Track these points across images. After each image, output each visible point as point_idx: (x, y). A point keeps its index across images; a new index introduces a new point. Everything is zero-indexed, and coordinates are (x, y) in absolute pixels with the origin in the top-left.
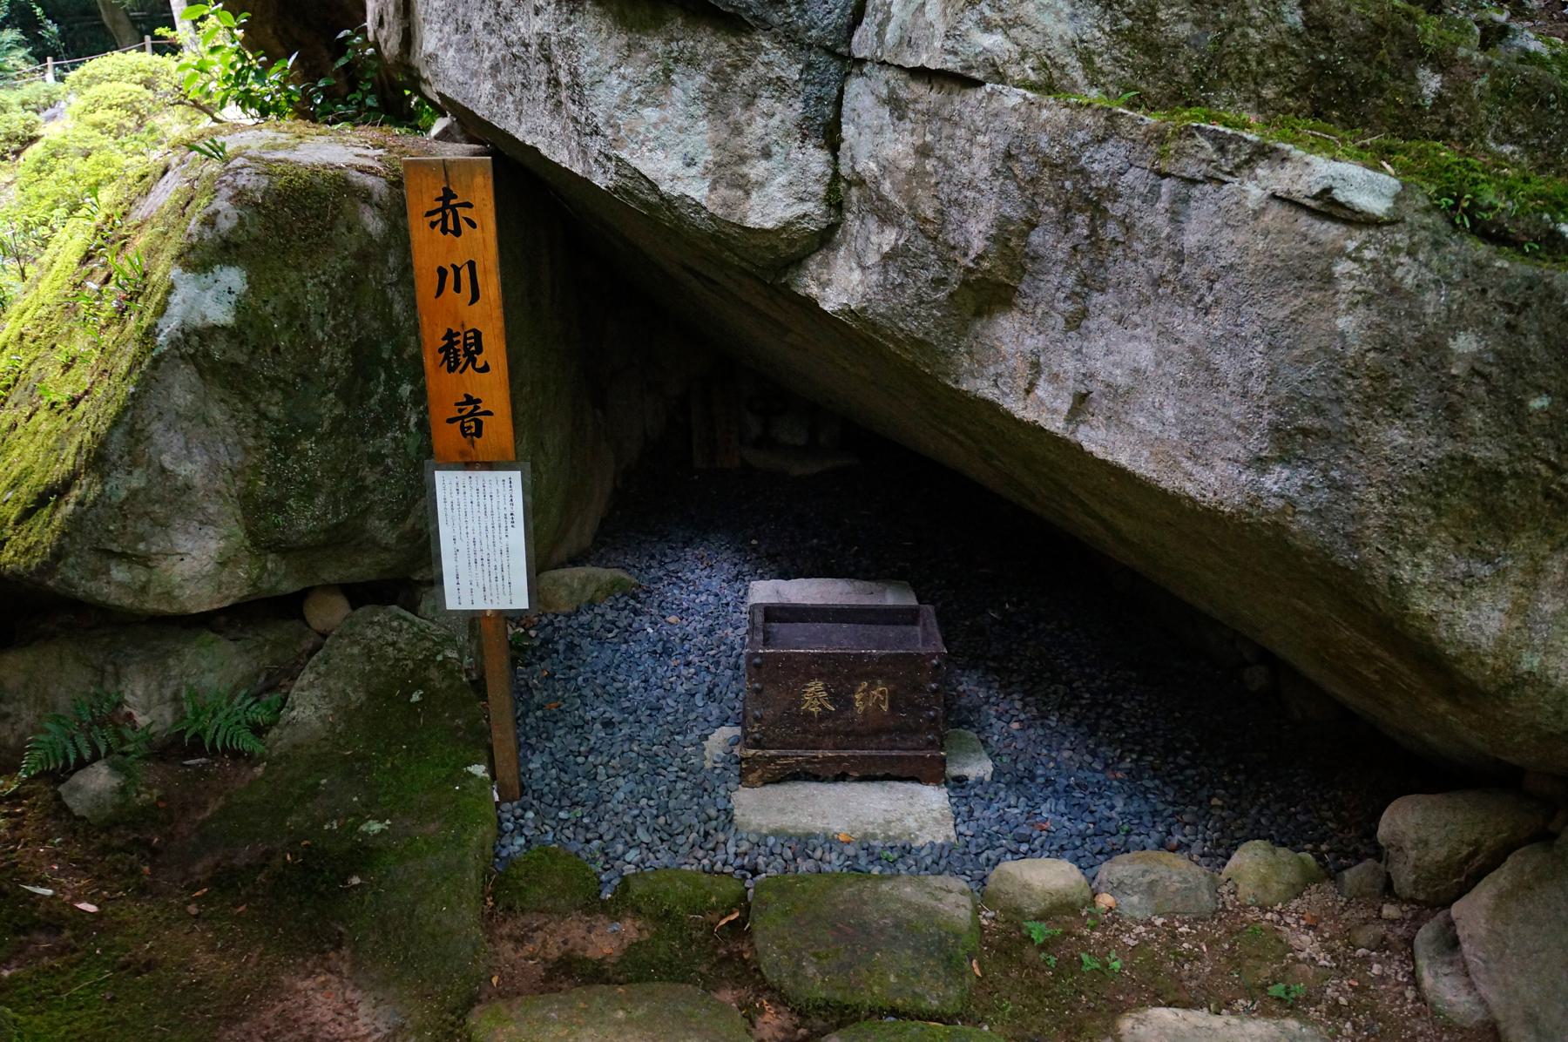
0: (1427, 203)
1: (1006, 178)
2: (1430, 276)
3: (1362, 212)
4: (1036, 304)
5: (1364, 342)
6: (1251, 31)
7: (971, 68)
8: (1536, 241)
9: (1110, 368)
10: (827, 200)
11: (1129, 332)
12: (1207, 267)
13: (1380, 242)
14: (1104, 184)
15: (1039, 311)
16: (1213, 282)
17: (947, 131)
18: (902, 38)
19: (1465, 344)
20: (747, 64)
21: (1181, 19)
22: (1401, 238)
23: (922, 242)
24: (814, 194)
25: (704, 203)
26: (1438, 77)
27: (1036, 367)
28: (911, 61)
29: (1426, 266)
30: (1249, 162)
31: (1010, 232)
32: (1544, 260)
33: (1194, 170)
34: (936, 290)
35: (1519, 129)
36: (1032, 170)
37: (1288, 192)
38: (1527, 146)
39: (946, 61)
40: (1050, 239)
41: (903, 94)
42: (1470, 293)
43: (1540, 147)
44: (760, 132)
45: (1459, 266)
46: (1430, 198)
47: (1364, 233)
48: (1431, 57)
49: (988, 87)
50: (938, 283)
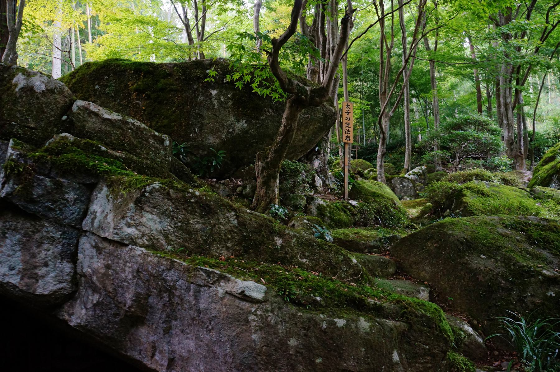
0: (275, 293)
1: (138, 279)
2: (279, 320)
3: (255, 299)
4: (153, 324)
5: (261, 343)
6: (221, 226)
7: (123, 240)
8: (310, 304)
9: (180, 349)
10: (71, 282)
11: (186, 336)
12: (208, 316)
13: (262, 308)
14: (172, 284)
15: (154, 327)
16: (211, 321)
17: (116, 261)
18: (100, 226)
19: (293, 342)
20: (39, 231)
21: (198, 223)
22: (268, 307)
23: (108, 300)
24: (66, 280)
25: (17, 285)
26: (281, 240)
27: (154, 348)
28: (103, 235)
29: (277, 316)
30: (218, 280)
31: (141, 298)
32: (313, 310)
33: (200, 282)
34: (115, 318)
35: (307, 254)
36: (147, 277)
37: (231, 291)
38: (310, 259)
39: (114, 237)
40: (156, 301)
41: (101, 245)
42: (292, 325)
43: (313, 259)
44: (43, 256)
45: (287, 315)
46: (276, 292)
47: (257, 305)
48: (278, 234)
49: (130, 246)
50: (116, 315)
